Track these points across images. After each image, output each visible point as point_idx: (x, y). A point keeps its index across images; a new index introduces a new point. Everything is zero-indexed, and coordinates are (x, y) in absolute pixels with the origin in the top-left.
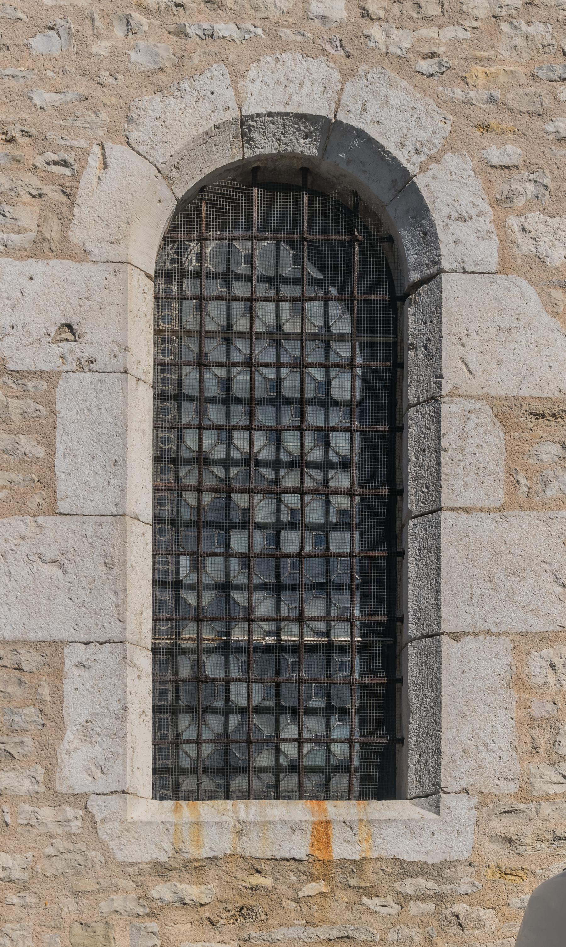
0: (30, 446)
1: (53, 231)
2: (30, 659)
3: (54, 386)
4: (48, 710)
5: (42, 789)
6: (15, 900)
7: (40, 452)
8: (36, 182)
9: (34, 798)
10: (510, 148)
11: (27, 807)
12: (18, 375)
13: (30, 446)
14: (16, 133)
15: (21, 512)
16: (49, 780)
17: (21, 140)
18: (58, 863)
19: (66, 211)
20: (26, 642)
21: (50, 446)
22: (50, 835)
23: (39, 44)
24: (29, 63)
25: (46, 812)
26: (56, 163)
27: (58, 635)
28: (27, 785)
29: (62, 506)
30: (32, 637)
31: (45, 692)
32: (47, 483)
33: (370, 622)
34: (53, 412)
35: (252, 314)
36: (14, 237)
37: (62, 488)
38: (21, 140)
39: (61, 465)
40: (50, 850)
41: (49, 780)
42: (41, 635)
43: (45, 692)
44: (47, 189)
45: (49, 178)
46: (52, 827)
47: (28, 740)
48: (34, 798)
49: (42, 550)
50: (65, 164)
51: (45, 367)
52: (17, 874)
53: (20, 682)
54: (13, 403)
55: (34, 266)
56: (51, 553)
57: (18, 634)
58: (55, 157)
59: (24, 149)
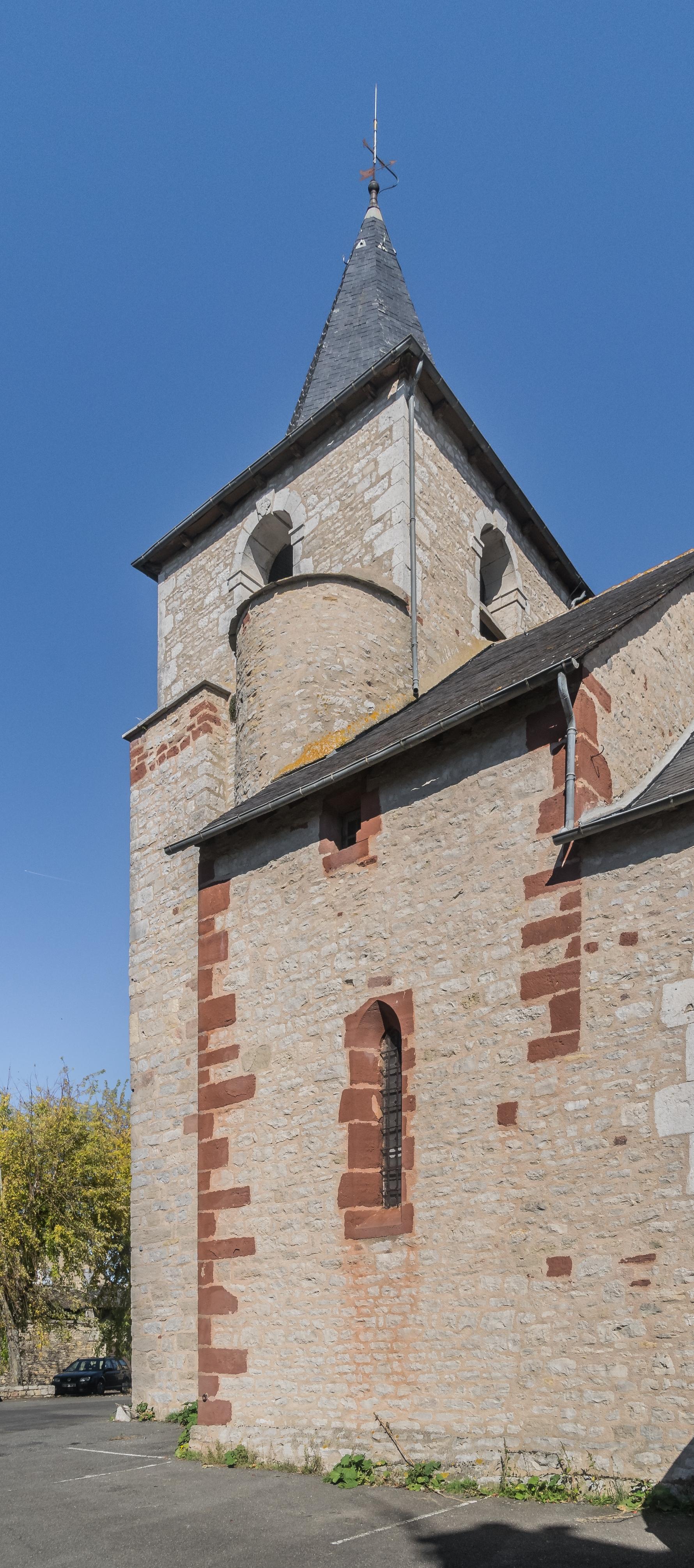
0: (676, 1057)
1: (684, 969)
2: (676, 1142)
3: (685, 1030)
4: (683, 1162)
5: (681, 1194)
6: (671, 1240)
7: (680, 1058)
8: (679, 950)
9: (678, 1198)
10: (646, 1459)
11: (675, 1202)
12: (672, 1029)
13: (676, 1057)
14: (670, 933)
15: (673, 1084)
16: (684, 1190)
17: (672, 935)
18: (687, 1223)
19: (690, 959)
20: (674, 1136)
21: (683, 1055)
22: (684, 1212)
23: (679, 894)
24: (676, 903)
25: (683, 1203)
26: (490, 685)
27: (687, 1131)
28: (675, 1193)
29: (688, 1078)
30: (677, 1133)
31: (682, 1154)
32: (682, 1070)
33: (576, 956)
34: (685, 1041)
35: (686, 703)
36: (669, 975)
37: (688, 1071)
38: (672, 935)
39: (688, 1062)
40: (684, 1219)
41: (684, 1190)
42: (680, 1132)
43: (682, 1154)
44: (682, 952)
45: (684, 947)
46: (685, 1209)
47: (675, 1174)
48: (678, 1198)
49: (681, 1097)
50: (689, 940)
51: (681, 1024)
52: (671, 1230)
53: (673, 1152)
54: (669, 1041)
55: (677, 984)
56: (683, 1098)
57: (671, 1133)
58: (685, 938)
59: (675, 939)
